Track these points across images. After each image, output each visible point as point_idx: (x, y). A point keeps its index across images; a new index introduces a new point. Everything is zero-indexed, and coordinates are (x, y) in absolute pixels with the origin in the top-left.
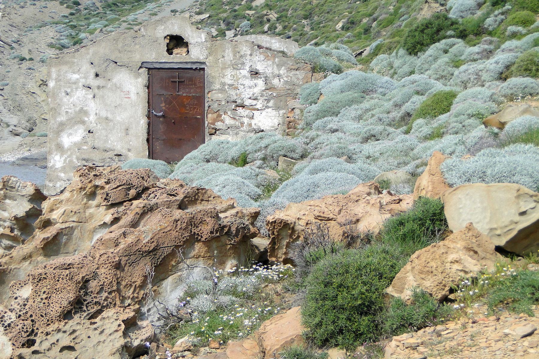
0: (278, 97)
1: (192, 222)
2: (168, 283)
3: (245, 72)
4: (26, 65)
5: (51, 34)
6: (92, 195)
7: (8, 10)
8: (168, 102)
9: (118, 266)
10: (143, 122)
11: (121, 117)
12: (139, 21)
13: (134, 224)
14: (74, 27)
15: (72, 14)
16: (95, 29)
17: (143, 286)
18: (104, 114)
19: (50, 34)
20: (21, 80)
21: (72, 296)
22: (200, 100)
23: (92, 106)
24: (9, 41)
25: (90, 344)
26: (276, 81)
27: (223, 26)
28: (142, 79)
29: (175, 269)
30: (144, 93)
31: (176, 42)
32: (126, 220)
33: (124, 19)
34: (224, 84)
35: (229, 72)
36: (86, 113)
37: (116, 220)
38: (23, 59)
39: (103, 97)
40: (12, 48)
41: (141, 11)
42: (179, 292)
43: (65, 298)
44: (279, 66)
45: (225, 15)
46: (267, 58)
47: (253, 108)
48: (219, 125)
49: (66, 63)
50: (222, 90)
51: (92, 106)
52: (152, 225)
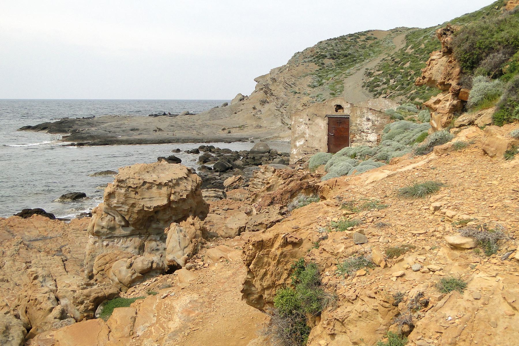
0: (376, 129)
1: (301, 184)
2: (295, 199)
3: (364, 119)
4: (297, 95)
5: (310, 80)
6: (280, 176)
7: (291, 67)
8: (336, 130)
9: (282, 194)
10: (326, 137)
11: (318, 135)
12: (351, 73)
13: (288, 185)
14: (320, 76)
15: (320, 69)
16: (330, 78)
17: (288, 199)
18: (311, 134)
19: (309, 80)
20: (294, 103)
21: (270, 201)
22: (348, 129)
23: (307, 131)
24: (290, 83)
25: (272, 212)
26: (376, 123)
27: (389, 77)
28: (326, 121)
29: (297, 195)
30: (326, 127)
31: (339, 107)
32: (287, 183)
33: (344, 72)
34: (356, 124)
35: (359, 119)
36: (305, 134)
37: (285, 183)
38: (296, 93)
39: (311, 128)
40: (291, 87)
41: (352, 68)
42: (297, 201)
43: (269, 201)
44: (378, 117)
45: (390, 72)
46: (373, 114)
47: (367, 133)
48: (354, 139)
49: (298, 115)
50: (356, 126)
51: (307, 131)
52: (292, 184)
